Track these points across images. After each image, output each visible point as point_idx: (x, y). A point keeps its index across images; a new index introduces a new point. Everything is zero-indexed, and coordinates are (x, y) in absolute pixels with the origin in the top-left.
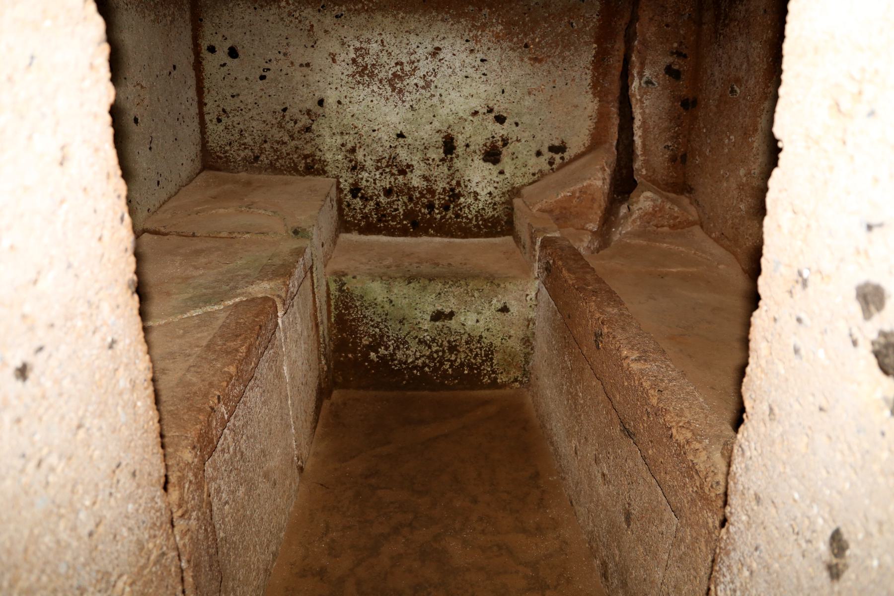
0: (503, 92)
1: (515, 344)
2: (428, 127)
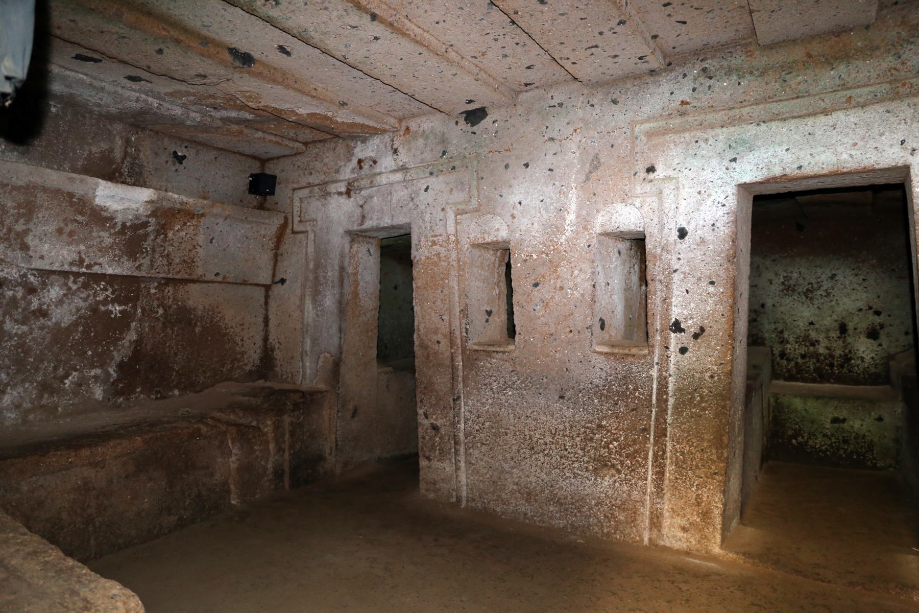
0: (879, 297)
2: (829, 318)
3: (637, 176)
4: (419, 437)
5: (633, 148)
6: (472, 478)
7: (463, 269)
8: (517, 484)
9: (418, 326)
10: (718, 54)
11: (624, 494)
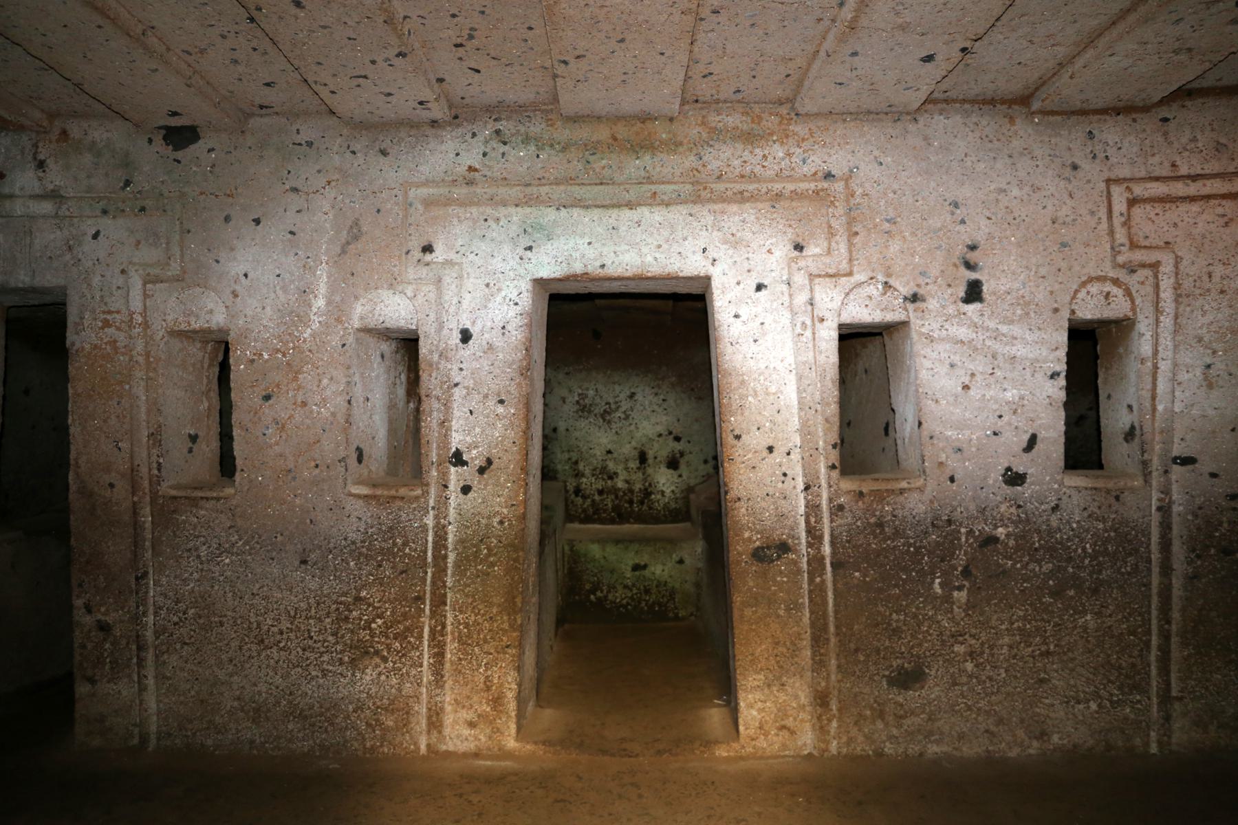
1: (689, 587)
2: (628, 446)
3: (409, 256)
4: (76, 645)
5: (406, 217)
6: (166, 700)
7: (154, 369)
8: (239, 699)
9: (76, 460)
10: (514, 116)
11: (393, 690)
